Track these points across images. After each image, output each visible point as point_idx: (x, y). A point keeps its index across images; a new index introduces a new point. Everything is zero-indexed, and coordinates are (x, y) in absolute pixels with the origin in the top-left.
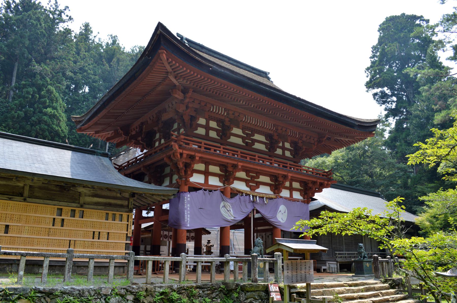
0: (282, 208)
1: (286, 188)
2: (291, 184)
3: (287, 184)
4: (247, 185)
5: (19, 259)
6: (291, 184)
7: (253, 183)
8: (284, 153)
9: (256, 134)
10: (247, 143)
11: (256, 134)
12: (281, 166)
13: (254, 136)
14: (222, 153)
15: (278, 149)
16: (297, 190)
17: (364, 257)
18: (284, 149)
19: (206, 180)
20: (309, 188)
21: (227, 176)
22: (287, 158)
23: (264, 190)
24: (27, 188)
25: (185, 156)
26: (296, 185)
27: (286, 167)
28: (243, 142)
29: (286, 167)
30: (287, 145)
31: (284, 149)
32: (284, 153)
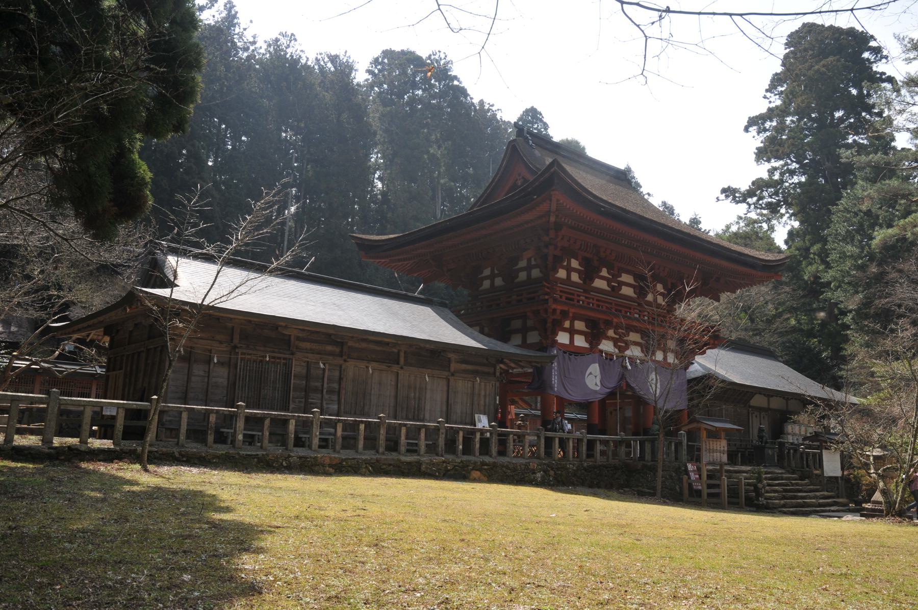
0: (595, 368)
1: (565, 330)
2: (572, 325)
3: (567, 324)
4: (615, 346)
5: (114, 414)
6: (572, 325)
7: (621, 344)
8: (569, 276)
9: (623, 275)
10: (613, 288)
11: (623, 275)
12: (564, 298)
13: (620, 276)
14: (585, 304)
15: (560, 270)
16: (580, 333)
17: (766, 443)
18: (569, 270)
19: (572, 340)
20: (690, 348)
21: (594, 336)
22: (575, 284)
23: (635, 352)
24: (402, 354)
25: (558, 312)
26: (579, 325)
27: (572, 300)
28: (608, 285)
29: (572, 300)
30: (575, 264)
31: (569, 270)
32: (569, 276)
